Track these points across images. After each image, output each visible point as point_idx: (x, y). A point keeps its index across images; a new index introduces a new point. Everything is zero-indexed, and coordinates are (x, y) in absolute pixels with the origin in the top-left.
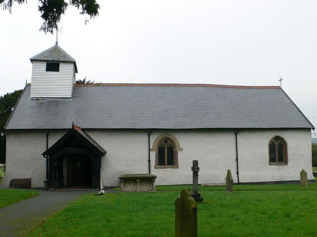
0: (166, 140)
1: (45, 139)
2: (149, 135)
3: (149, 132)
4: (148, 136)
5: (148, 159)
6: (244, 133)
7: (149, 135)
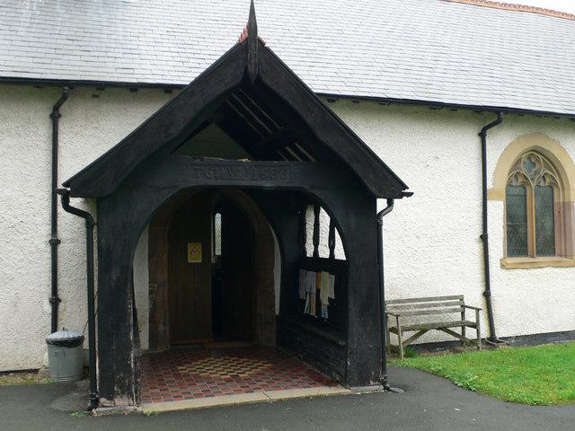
0: (536, 156)
1: (44, 130)
2: (55, 118)
3: (487, 119)
4: (477, 141)
5: (479, 232)
6: (428, 124)
7: (55, 118)
